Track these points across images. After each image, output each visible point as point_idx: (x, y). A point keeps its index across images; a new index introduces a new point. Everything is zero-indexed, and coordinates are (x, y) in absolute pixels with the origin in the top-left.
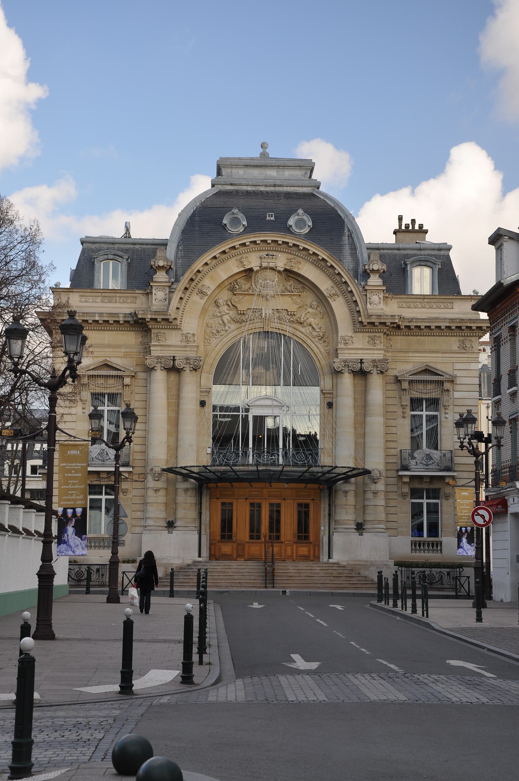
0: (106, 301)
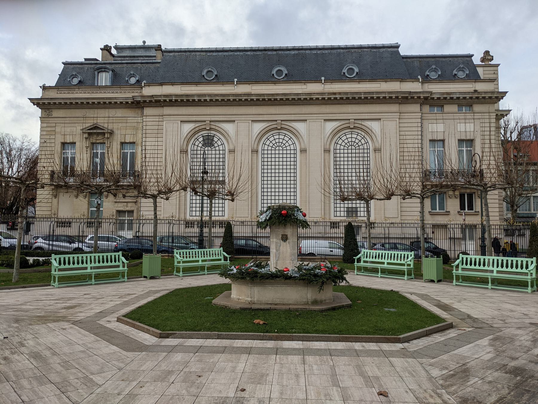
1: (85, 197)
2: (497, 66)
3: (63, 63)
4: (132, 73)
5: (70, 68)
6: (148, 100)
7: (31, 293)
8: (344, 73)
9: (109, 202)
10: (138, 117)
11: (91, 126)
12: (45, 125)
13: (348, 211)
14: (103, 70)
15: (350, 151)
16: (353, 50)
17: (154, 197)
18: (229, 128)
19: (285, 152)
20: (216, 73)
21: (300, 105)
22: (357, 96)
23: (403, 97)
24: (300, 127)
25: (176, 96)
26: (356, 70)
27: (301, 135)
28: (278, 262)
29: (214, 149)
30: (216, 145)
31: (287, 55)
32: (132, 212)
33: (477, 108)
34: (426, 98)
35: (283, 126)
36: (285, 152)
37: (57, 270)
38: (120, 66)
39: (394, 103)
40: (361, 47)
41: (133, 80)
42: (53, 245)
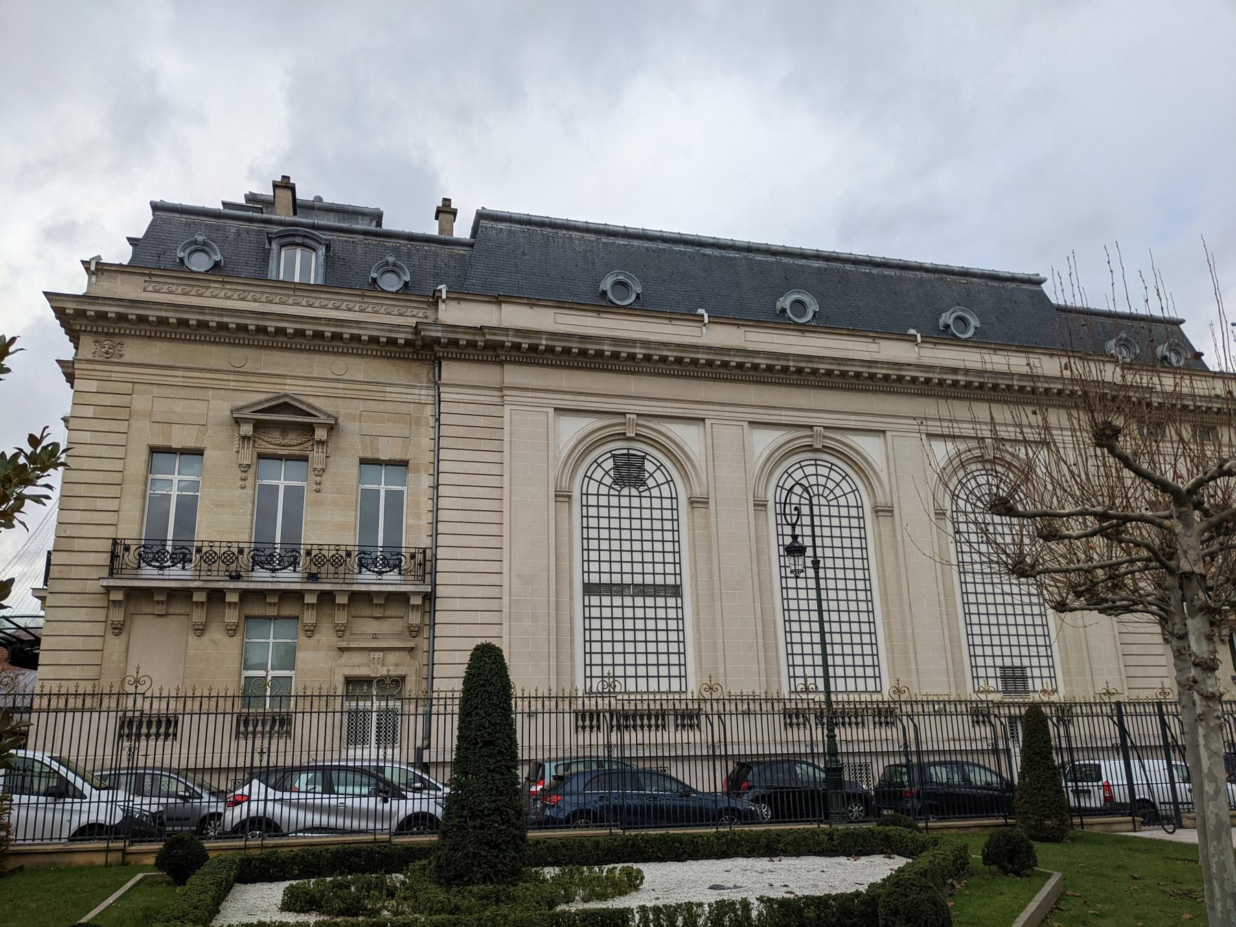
0: (150, 288)
1: (232, 631)
3: (156, 207)
6: (463, 338)
9: (317, 649)
10: (421, 388)
11: (267, 401)
13: (1003, 677)
16: (949, 278)
19: (834, 511)
24: (869, 447)
29: (647, 493)
30: (651, 483)
31: (803, 269)
32: (399, 681)
40: (965, 273)
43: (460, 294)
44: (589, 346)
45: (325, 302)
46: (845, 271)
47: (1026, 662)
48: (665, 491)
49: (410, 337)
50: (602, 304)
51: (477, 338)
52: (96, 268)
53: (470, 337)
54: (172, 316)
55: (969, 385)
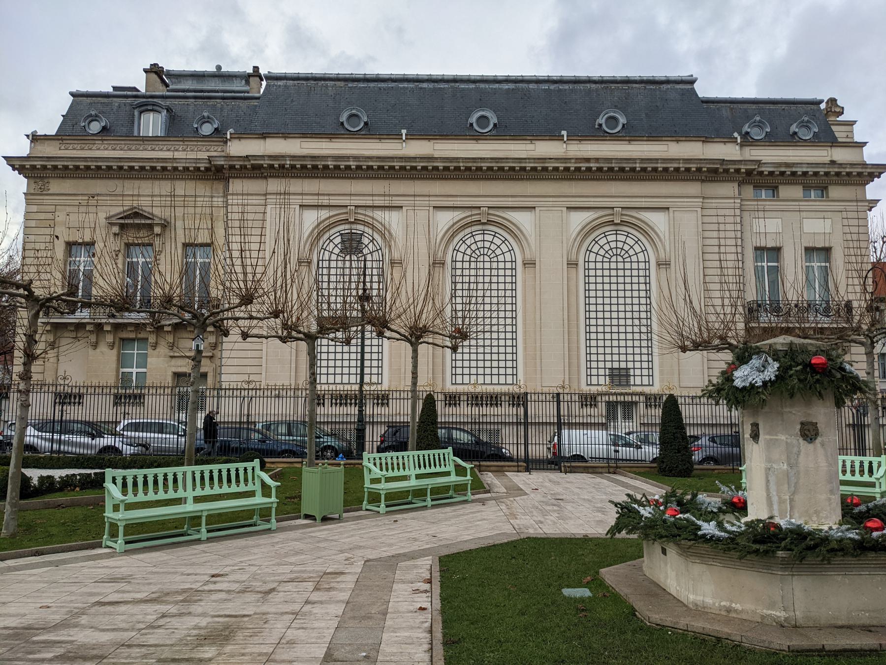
1: (112, 346)
2: (852, 123)
3: (72, 94)
4: (206, 114)
5: (85, 105)
7: (61, 574)
8: (600, 125)
9: (158, 357)
12: (34, 208)
14: (150, 108)
15: (613, 266)
16: (613, 86)
17: (310, 338)
18: (393, 220)
19: (628, 266)
20: (365, 119)
21: (522, 179)
22: (627, 166)
23: (710, 170)
24: (523, 219)
25: (293, 157)
26: (622, 120)
27: (524, 235)
28: (797, 498)
33: (835, 192)
34: (749, 173)
35: (492, 218)
36: (495, 265)
37: (122, 507)
38: (183, 101)
39: (693, 180)
41: (207, 129)
42: (60, 442)
43: (239, 136)
44: (318, 163)
45: (169, 147)
46: (528, 90)
47: (630, 365)
48: (641, 257)
49: (207, 165)
50: (338, 132)
51: (246, 163)
52: (35, 138)
53: (241, 163)
54: (71, 164)
55: (600, 169)
